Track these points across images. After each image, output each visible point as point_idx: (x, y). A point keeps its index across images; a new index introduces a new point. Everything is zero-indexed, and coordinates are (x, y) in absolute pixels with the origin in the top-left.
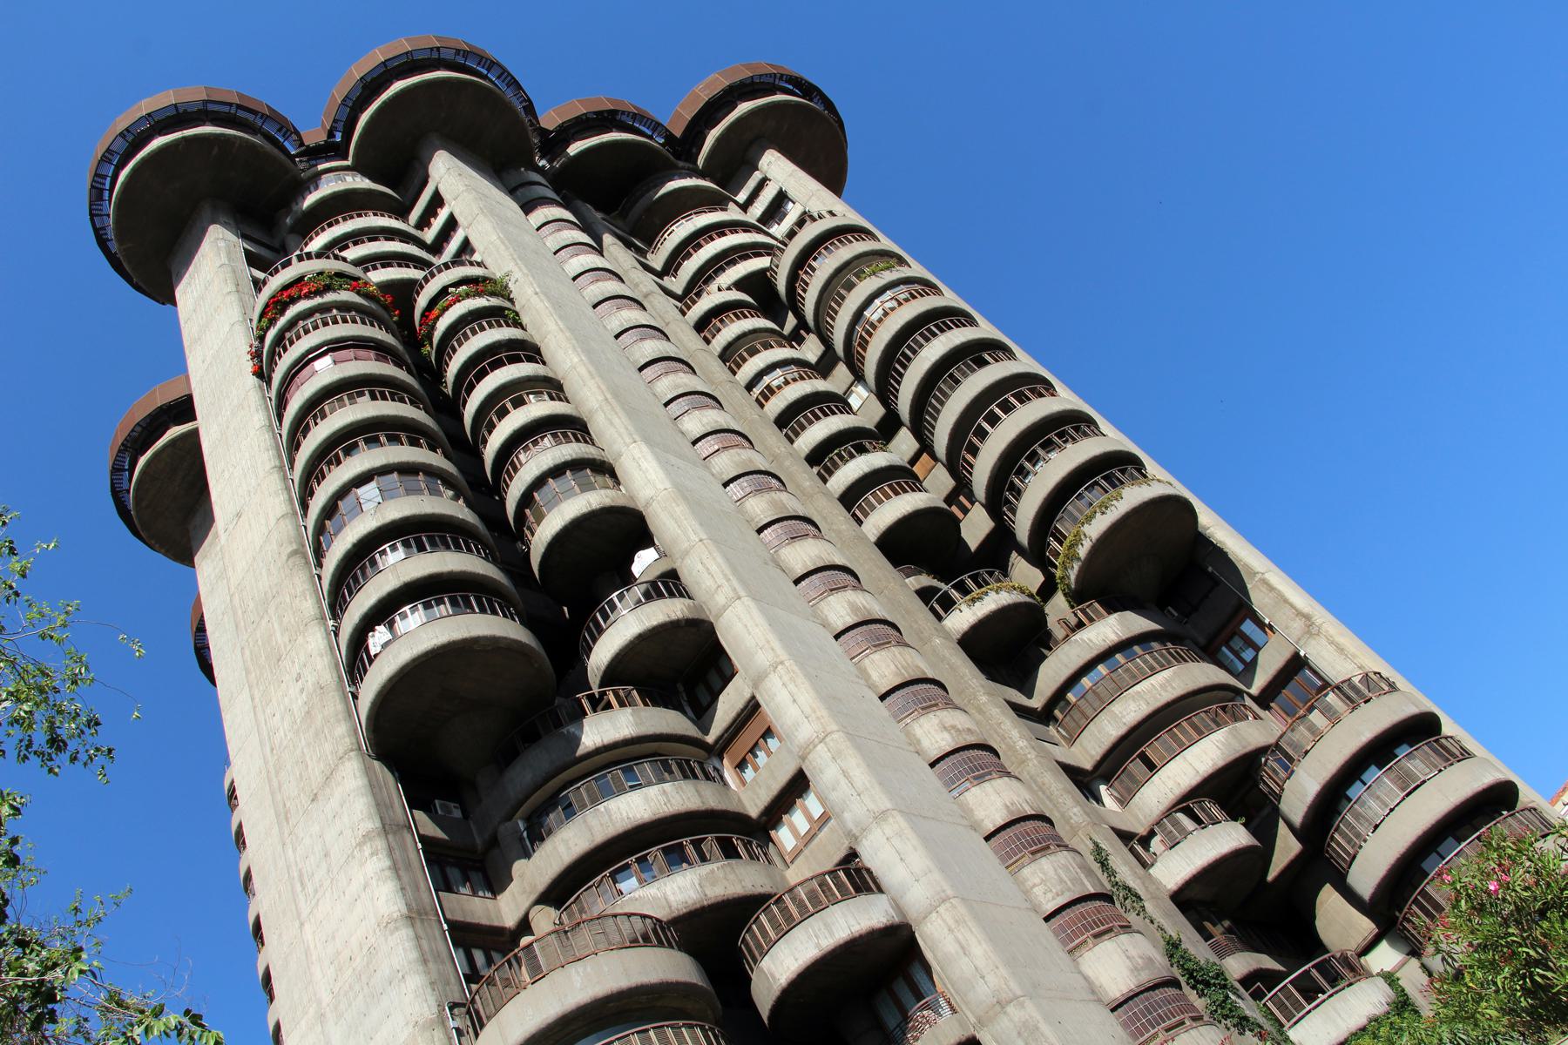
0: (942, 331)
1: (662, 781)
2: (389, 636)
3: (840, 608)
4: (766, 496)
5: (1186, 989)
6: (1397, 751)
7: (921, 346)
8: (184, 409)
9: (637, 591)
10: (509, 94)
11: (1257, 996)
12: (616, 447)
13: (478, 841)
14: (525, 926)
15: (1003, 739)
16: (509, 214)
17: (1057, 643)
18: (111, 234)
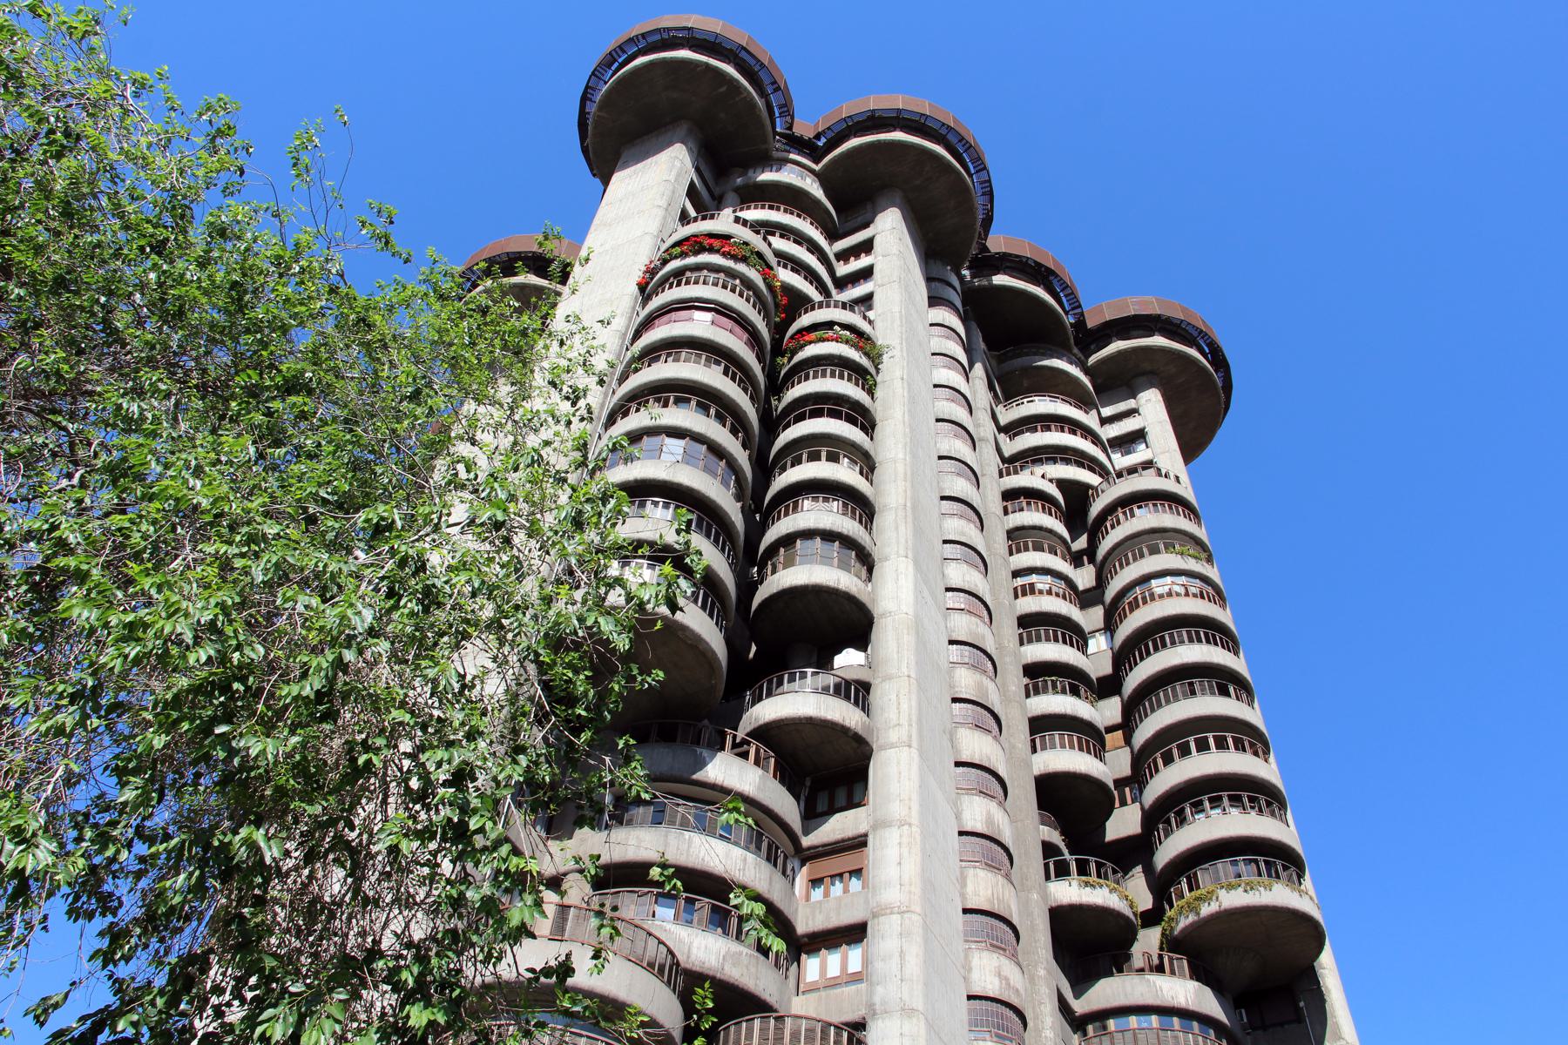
0: (1208, 642)
1: (747, 848)
3: (979, 812)
4: (978, 676)
7: (1182, 642)
10: (979, 201)
12: (887, 550)
14: (555, 883)
15: (1036, 1018)
16: (918, 298)
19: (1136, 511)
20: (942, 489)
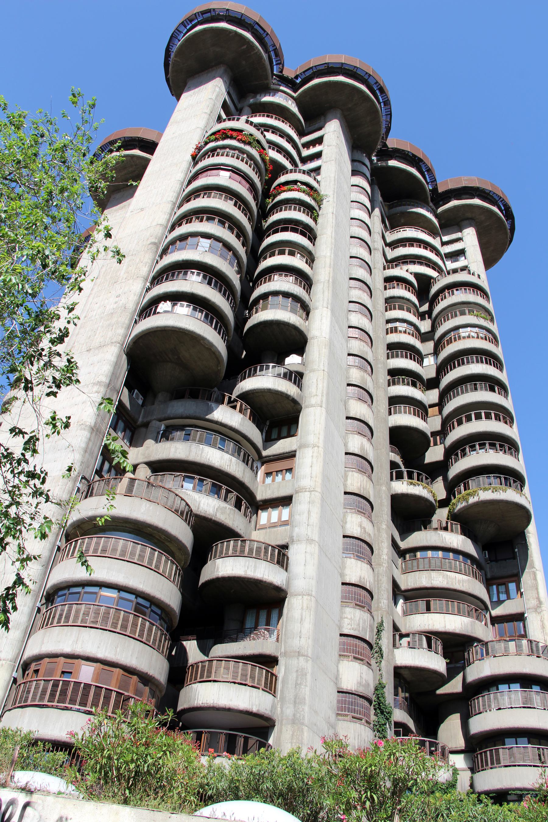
0: (487, 363)
1: (233, 455)
2: (169, 309)
3: (357, 443)
5: (372, 707)
6: (533, 686)
7: (473, 362)
8: (150, 147)
9: (282, 370)
10: (383, 119)
11: (397, 733)
13: (140, 420)
15: (379, 549)
17: (430, 528)
18: (174, 49)
19: (455, 291)
20: (350, 274)
